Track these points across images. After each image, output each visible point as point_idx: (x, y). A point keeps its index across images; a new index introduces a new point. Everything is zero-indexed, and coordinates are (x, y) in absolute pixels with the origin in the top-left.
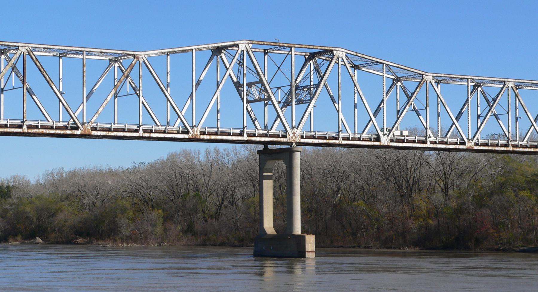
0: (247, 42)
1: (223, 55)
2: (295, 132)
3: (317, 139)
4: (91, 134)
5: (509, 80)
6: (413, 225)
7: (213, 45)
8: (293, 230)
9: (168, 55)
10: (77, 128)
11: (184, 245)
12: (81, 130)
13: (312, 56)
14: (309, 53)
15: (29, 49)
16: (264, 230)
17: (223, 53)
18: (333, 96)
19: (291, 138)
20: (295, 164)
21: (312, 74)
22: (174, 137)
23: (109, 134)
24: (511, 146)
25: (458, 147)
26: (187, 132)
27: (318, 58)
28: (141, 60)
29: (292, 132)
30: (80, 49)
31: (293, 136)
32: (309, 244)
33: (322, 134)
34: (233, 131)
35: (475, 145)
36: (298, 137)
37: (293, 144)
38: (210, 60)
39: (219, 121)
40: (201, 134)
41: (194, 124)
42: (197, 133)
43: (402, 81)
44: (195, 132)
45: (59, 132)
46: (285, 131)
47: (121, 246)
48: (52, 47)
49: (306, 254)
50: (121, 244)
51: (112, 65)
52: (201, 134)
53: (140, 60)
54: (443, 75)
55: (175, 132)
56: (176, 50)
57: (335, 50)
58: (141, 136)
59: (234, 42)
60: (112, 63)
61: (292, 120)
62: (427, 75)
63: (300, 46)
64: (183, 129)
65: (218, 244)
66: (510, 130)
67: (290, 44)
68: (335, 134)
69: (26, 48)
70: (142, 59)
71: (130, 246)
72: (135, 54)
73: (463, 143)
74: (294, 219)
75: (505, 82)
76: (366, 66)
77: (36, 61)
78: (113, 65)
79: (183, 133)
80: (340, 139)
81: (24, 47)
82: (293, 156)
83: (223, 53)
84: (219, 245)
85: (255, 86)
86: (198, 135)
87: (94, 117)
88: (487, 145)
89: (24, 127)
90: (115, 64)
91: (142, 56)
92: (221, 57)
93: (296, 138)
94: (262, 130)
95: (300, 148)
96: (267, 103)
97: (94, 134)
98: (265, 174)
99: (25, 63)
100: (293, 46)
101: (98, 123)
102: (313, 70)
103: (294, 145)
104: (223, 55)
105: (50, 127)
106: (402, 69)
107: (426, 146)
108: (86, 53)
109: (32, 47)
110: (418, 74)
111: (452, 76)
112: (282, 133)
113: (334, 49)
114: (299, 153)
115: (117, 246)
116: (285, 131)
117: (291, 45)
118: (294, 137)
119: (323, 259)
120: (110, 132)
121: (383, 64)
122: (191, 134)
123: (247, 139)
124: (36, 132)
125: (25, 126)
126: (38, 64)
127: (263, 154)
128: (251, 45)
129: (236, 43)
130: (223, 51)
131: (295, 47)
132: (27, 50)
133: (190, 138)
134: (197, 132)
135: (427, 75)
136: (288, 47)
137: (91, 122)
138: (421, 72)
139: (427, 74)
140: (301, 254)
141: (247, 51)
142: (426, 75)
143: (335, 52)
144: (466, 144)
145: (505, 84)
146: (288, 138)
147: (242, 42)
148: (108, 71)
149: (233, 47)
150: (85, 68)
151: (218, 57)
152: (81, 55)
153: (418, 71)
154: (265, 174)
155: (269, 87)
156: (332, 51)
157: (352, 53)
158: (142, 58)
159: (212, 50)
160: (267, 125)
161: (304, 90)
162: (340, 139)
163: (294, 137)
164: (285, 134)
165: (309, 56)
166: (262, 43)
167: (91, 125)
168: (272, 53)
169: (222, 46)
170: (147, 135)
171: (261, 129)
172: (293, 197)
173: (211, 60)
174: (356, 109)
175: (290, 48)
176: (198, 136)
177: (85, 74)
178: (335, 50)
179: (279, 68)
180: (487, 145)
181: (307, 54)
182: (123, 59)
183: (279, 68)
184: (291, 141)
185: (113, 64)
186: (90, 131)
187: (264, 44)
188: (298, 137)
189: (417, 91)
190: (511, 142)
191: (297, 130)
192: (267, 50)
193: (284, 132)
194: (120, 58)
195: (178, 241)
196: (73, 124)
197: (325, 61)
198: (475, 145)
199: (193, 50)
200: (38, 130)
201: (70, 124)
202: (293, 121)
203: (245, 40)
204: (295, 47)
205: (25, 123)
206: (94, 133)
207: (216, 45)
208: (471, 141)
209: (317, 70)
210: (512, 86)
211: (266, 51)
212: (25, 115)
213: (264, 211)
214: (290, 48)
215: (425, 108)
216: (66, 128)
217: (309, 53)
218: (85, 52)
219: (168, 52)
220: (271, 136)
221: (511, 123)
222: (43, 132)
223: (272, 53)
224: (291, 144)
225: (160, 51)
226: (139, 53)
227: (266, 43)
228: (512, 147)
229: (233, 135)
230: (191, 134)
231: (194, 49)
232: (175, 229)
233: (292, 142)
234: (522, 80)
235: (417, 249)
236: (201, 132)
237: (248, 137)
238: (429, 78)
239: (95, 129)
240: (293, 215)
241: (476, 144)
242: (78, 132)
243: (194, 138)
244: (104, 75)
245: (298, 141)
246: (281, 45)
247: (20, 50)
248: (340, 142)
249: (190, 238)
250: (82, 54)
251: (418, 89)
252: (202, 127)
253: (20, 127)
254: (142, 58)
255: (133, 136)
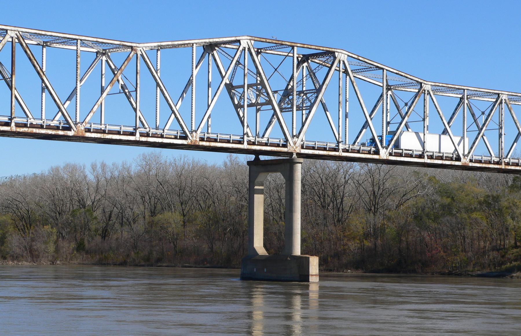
0: (249, 38)
1: (215, 52)
2: (296, 141)
3: (317, 150)
4: (85, 136)
5: (503, 92)
6: (353, 246)
7: (205, 41)
8: (293, 251)
9: (158, 50)
10: (69, 129)
11: (79, 264)
12: (74, 130)
13: (306, 58)
14: (302, 55)
15: (18, 34)
16: (254, 250)
17: (216, 50)
18: (325, 103)
19: (292, 147)
20: (296, 177)
21: (304, 80)
22: (172, 142)
23: (104, 136)
24: (503, 164)
25: (454, 163)
26: (185, 138)
27: (311, 61)
28: (139, 53)
29: (293, 141)
30: (74, 37)
31: (293, 145)
32: (313, 267)
33: (322, 145)
34: (233, 138)
35: (470, 162)
36: (299, 147)
37: (293, 154)
38: (201, 57)
39: (210, 127)
40: (200, 140)
41: (194, 129)
42: (196, 139)
43: (393, 90)
44: (194, 138)
45: (50, 132)
46: (285, 140)
47: (11, 264)
48: (43, 33)
49: (310, 277)
50: (11, 262)
51: (99, 59)
52: (200, 140)
53: (138, 53)
54: (441, 85)
55: (173, 137)
56: (176, 43)
57: (337, 52)
58: (138, 140)
59: (235, 37)
60: (99, 56)
61: (293, 128)
62: (426, 84)
63: (302, 45)
64: (181, 133)
65: (118, 263)
66: (503, 147)
67: (293, 43)
68: (335, 145)
69: (16, 32)
70: (140, 52)
71: (21, 264)
72: (133, 46)
73: (458, 159)
74: (294, 238)
75: (499, 94)
76: (359, 72)
77: (25, 49)
78: (101, 59)
79: (181, 138)
80: (341, 150)
81: (13, 32)
82: (294, 168)
83: (216, 50)
84: (119, 265)
85: (253, 88)
86: (197, 141)
87: (89, 116)
88: (480, 162)
89: (12, 125)
90: (102, 58)
91: (140, 48)
92: (213, 55)
93: (296, 148)
94: (253, 137)
95: (301, 160)
96: (259, 109)
97: (87, 136)
98: (256, 187)
99: (14, 50)
100: (295, 45)
101: (92, 124)
102: (306, 76)
103: (295, 155)
104: (215, 52)
105: (40, 126)
106: (402, 75)
107: (423, 162)
108: (81, 43)
109: (22, 32)
110: (416, 82)
111: (450, 86)
112: (282, 142)
113: (336, 50)
114: (300, 164)
115: (7, 264)
116: (285, 140)
117: (293, 44)
118: (295, 147)
119: (328, 283)
120: (105, 135)
121: (383, 69)
122: (190, 139)
123: (248, 147)
124: (24, 132)
125: (13, 124)
126: (29, 52)
127: (255, 165)
128: (253, 42)
129: (238, 38)
130: (216, 48)
131: (297, 47)
132: (16, 34)
133: (189, 144)
134: (196, 138)
135: (426, 84)
136: (291, 46)
137: (85, 122)
138: (420, 80)
139: (425, 82)
140: (305, 277)
141: (249, 49)
142: (425, 84)
143: (336, 54)
144: (462, 161)
145: (499, 97)
146: (289, 148)
147: (244, 38)
148: (95, 65)
149: (225, 45)
150: (79, 60)
151: (211, 54)
152: (65, 44)
153: (417, 79)
154: (256, 187)
155: (270, 90)
156: (334, 52)
157: (354, 56)
158: (140, 50)
159: (203, 46)
160: (258, 134)
161: (301, 95)
162: (340, 151)
163: (295, 147)
164: (285, 143)
165: (302, 58)
166: (264, 40)
167: (85, 125)
168: (265, 53)
169: (223, 41)
170: (144, 139)
171: (252, 136)
172: (294, 213)
173: (203, 57)
174: (347, 119)
175: (291, 47)
176: (197, 143)
177: (79, 66)
178: (337, 52)
179: (276, 70)
180: (480, 162)
181: (300, 55)
182: (112, 51)
183: (276, 70)
184: (291, 152)
185: (100, 57)
186: (84, 132)
187: (266, 42)
188: (299, 147)
189: (416, 101)
190: (504, 159)
191: (297, 139)
192: (261, 49)
193: (284, 141)
194: (108, 51)
195: (71, 259)
196: (65, 123)
197: (321, 66)
198: (470, 162)
199: (193, 44)
200: (27, 129)
201: (62, 123)
202: (294, 129)
203: (247, 36)
204: (297, 47)
205: (13, 121)
206: (88, 135)
207: (207, 41)
208: (466, 157)
209: (312, 74)
210: (505, 100)
211: (259, 51)
212: (13, 110)
213: (255, 228)
214: (291, 47)
215: (422, 120)
216: (57, 128)
217: (302, 55)
218: (79, 41)
219: (159, 46)
220: (272, 145)
221: (504, 140)
222: (32, 132)
223: (265, 53)
224: (291, 154)
225: (159, 44)
226: (138, 45)
227: (268, 41)
228: (505, 165)
229: (232, 143)
230: (190, 139)
231: (195, 43)
232: (67, 246)
233: (293, 153)
234: (515, 93)
235: (360, 273)
236: (200, 137)
237: (248, 146)
238: (427, 87)
239: (88, 130)
240: (293, 234)
241: (471, 161)
242: (70, 133)
243: (192, 144)
244: (91, 70)
245: (298, 151)
246: (283, 43)
247: (8, 34)
248: (340, 154)
249: (85, 256)
250: (75, 44)
251: (417, 99)
252: (201, 132)
253: (7, 124)
254: (140, 50)
255: (129, 139)
